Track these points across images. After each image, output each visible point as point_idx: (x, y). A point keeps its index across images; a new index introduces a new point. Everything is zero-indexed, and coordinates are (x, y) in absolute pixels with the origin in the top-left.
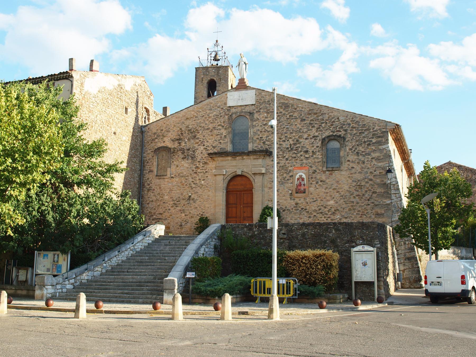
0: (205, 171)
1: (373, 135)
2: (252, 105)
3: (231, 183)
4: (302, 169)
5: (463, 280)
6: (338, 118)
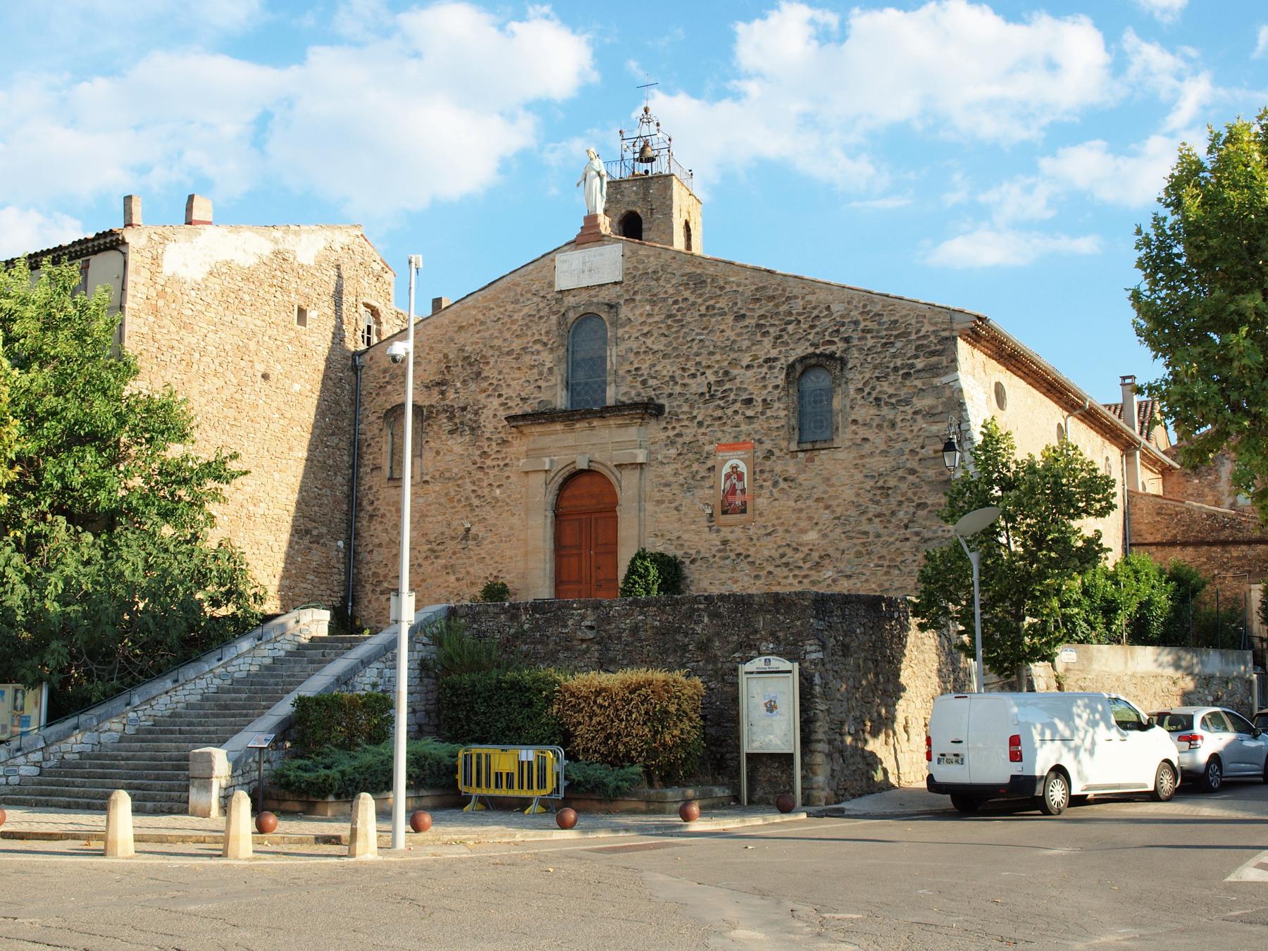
0: (502, 464)
1: (917, 348)
2: (616, 283)
3: (567, 493)
4: (738, 449)
5: (1014, 749)
6: (828, 308)
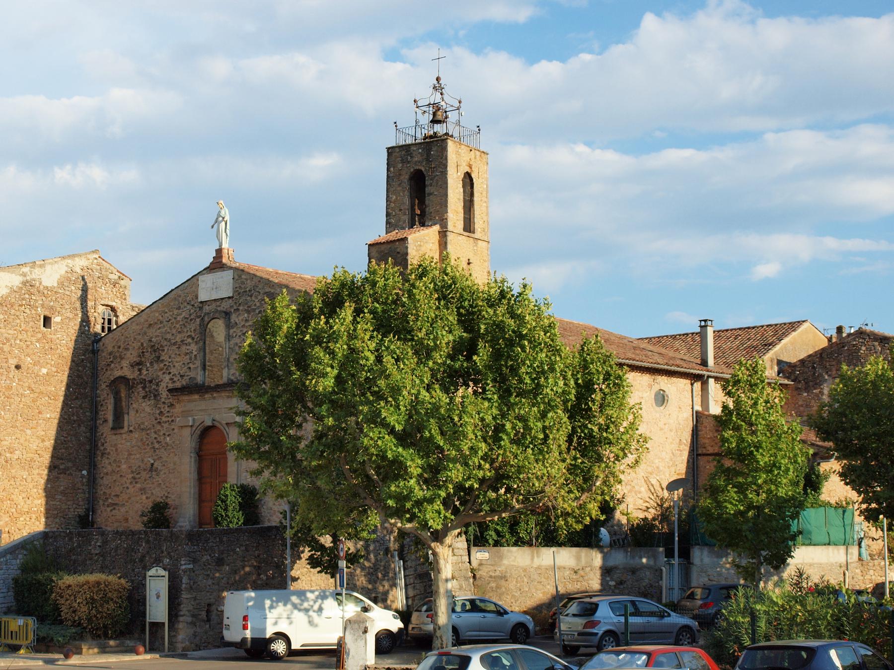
2: (229, 298)
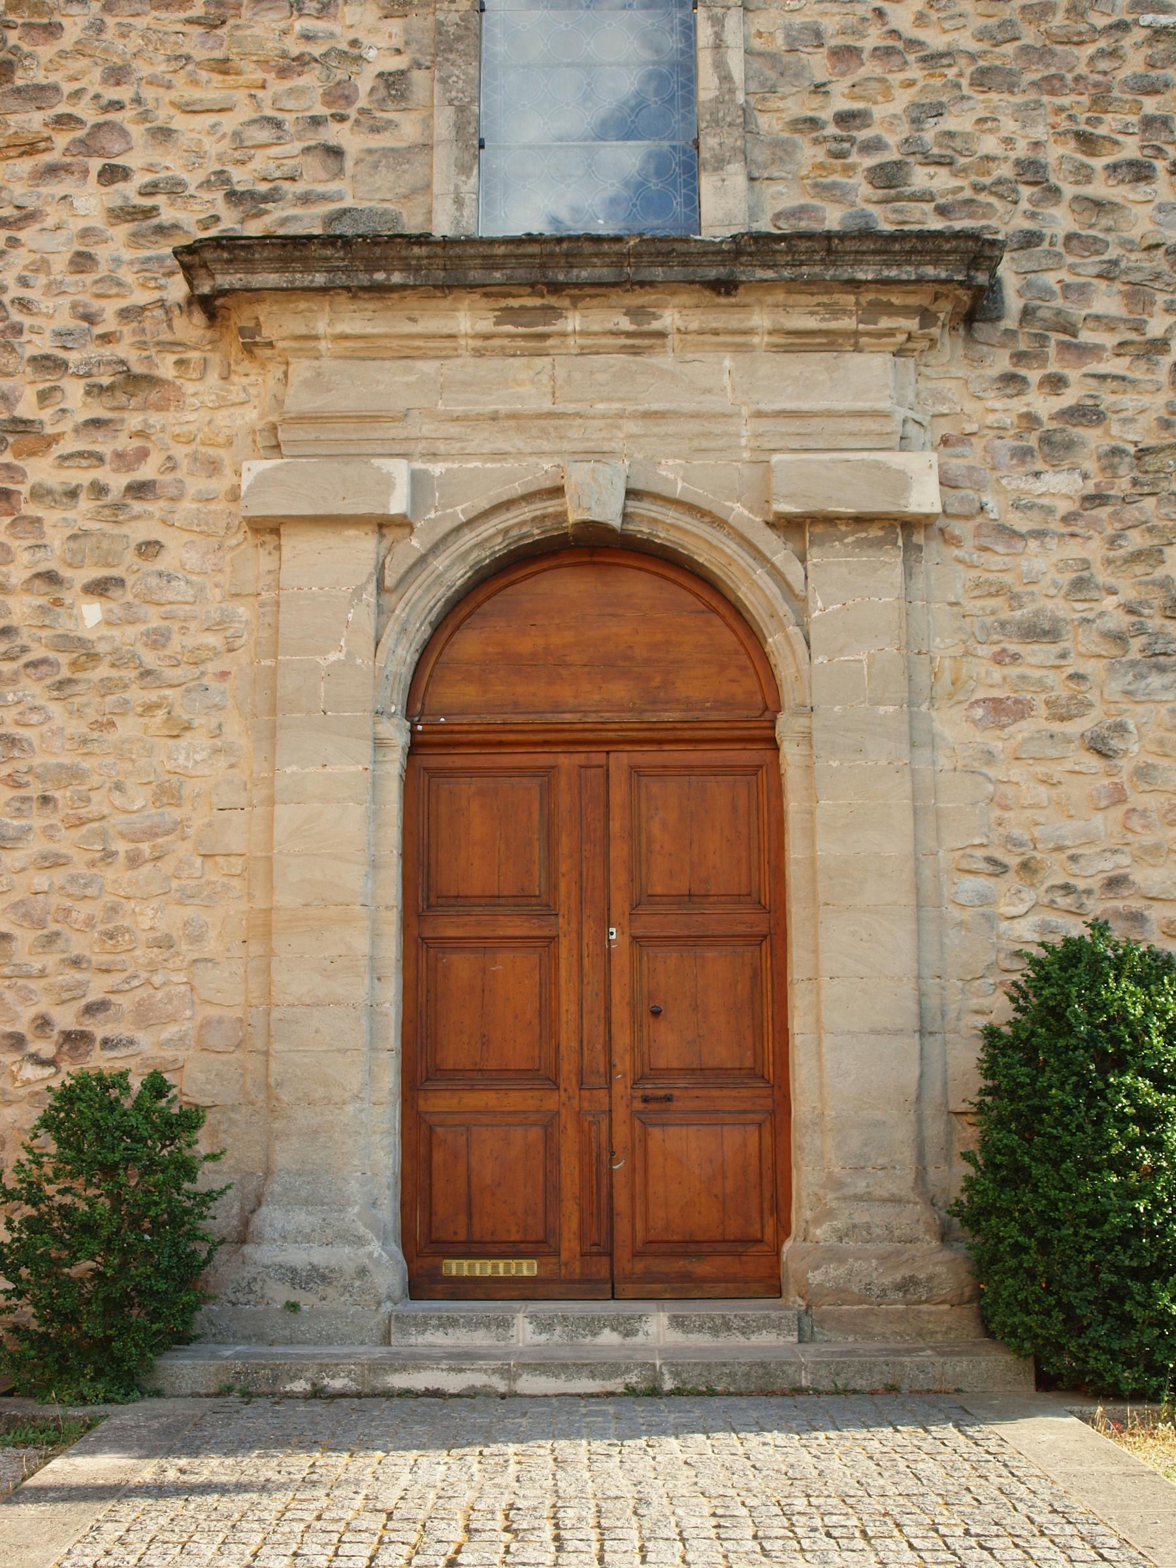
0: (117, 482)
3: (469, 644)
